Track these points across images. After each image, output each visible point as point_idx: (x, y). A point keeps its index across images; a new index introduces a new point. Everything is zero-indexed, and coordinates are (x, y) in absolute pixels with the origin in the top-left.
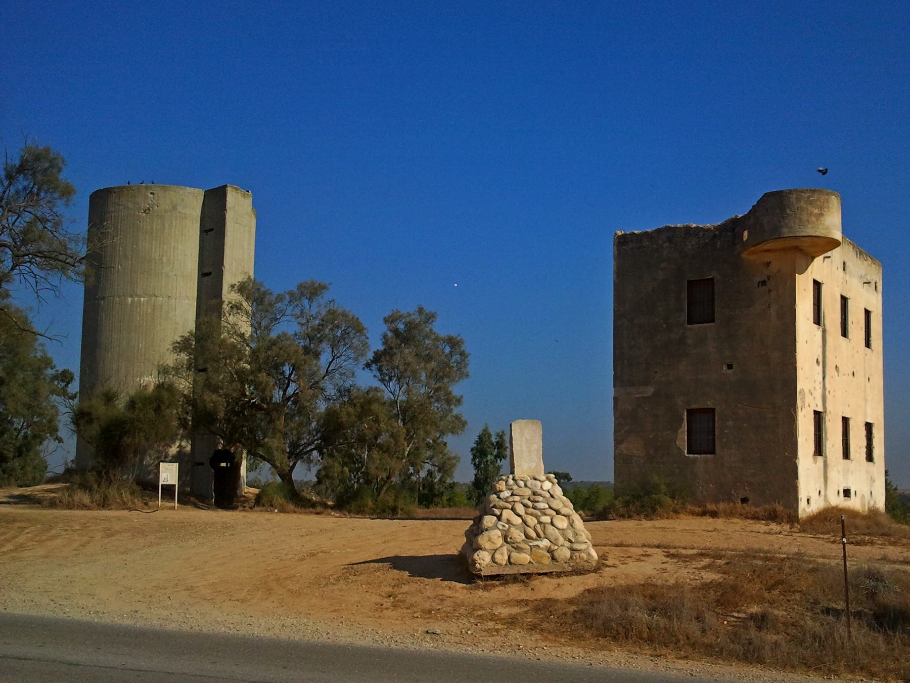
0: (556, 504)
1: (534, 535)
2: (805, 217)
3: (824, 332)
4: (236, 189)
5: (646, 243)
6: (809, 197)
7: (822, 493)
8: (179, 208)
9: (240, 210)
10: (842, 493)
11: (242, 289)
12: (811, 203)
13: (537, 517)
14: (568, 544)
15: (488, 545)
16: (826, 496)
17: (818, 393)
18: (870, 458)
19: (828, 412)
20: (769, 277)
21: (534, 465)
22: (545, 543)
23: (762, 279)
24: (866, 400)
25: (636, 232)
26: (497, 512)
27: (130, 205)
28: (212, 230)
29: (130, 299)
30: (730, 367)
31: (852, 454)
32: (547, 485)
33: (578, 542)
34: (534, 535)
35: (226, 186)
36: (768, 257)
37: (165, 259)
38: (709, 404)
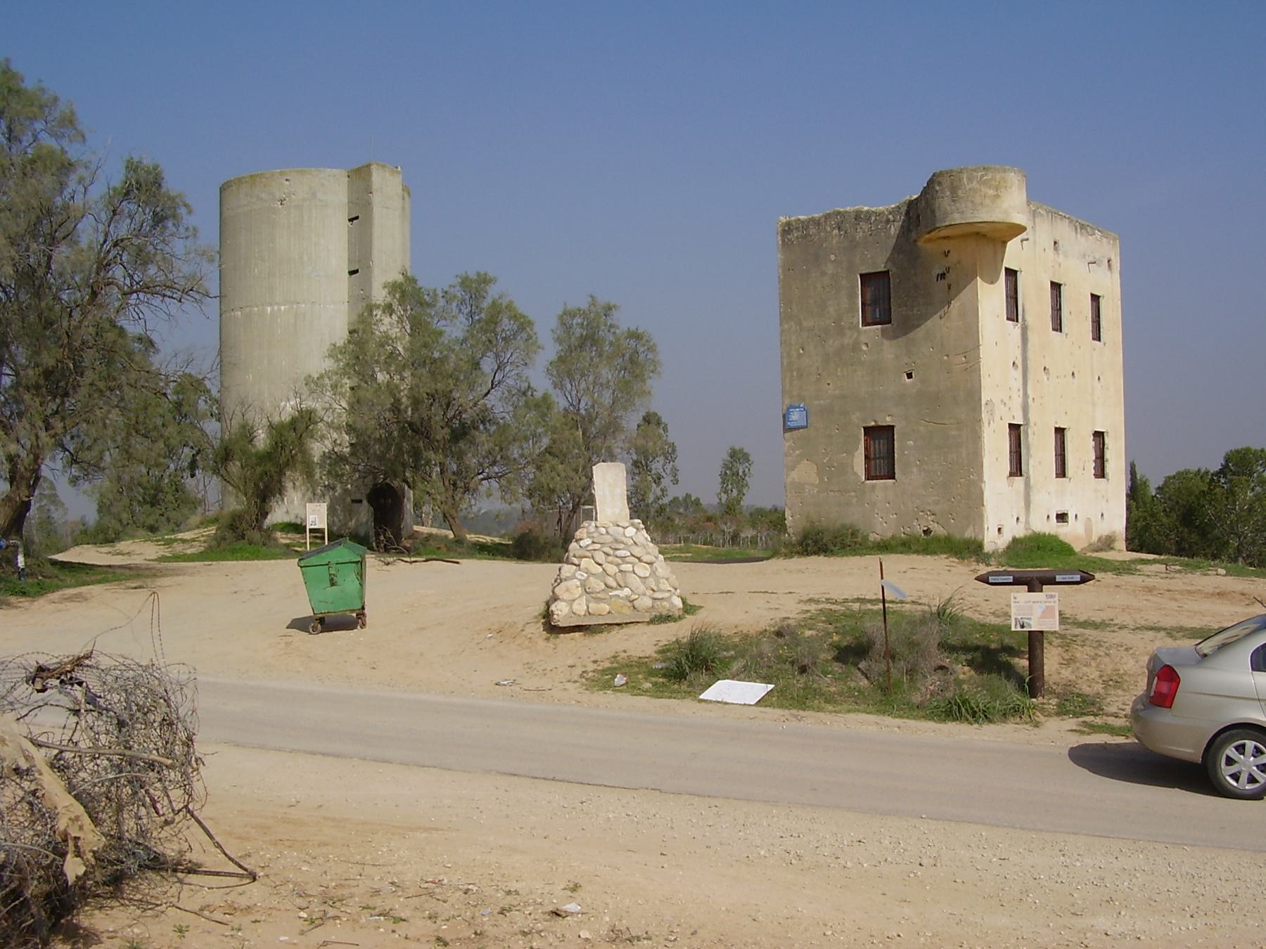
0: (637, 551)
1: (614, 584)
2: (978, 199)
3: (1024, 330)
4: (383, 166)
5: (812, 231)
6: (982, 176)
7: (1022, 519)
8: (319, 195)
9: (387, 187)
10: (1053, 518)
11: (394, 288)
12: (986, 183)
13: (618, 565)
14: (649, 592)
15: (565, 596)
16: (1027, 522)
17: (1017, 401)
18: (1101, 472)
19: (1032, 423)
20: (948, 270)
21: (617, 511)
22: (627, 591)
23: (940, 272)
24: (1094, 404)
25: (802, 217)
26: (576, 561)
27: (263, 196)
28: (357, 218)
29: (269, 309)
30: (909, 376)
31: (1109, 468)
32: (631, 531)
33: (660, 590)
34: (614, 584)
35: (369, 166)
36: (946, 245)
37: (305, 258)
38: (888, 421)
